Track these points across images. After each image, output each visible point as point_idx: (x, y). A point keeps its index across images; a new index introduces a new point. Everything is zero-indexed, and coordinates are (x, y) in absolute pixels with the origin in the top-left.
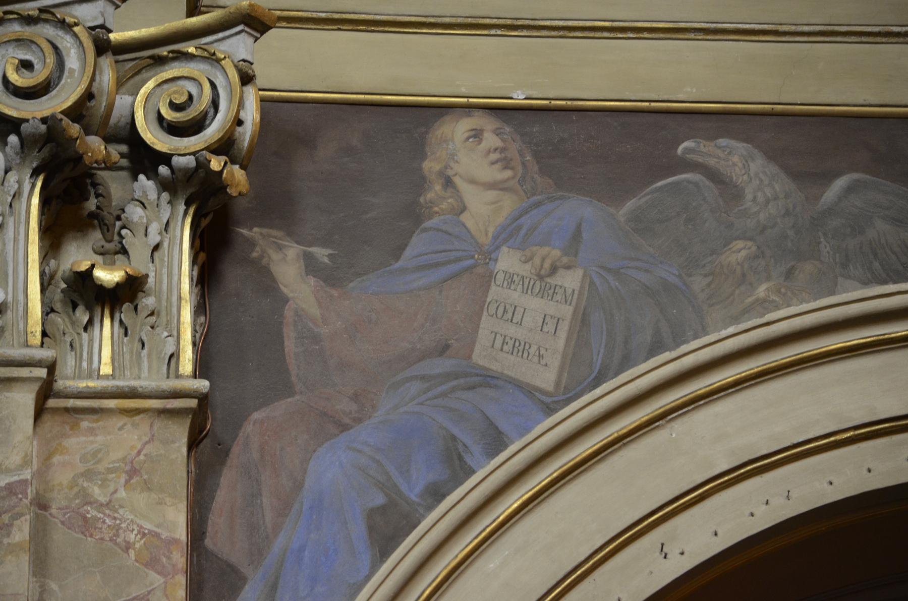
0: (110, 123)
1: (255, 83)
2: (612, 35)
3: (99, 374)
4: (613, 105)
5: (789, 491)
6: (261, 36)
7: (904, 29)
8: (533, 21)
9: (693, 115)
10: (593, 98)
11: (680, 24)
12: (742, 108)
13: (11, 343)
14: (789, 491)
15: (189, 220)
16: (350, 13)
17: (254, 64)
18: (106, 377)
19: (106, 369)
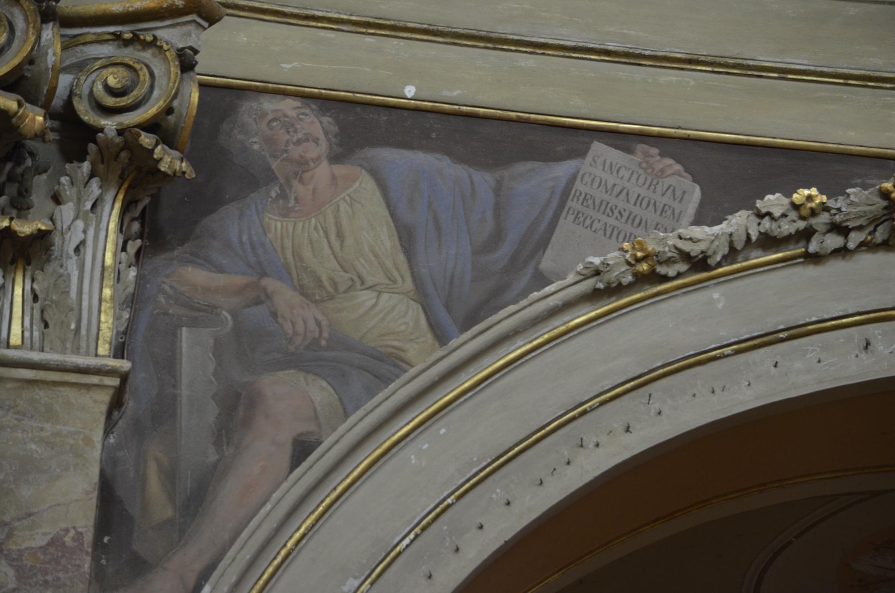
0: (53, 103)
1: (194, 70)
2: (393, 33)
3: (8, 343)
4: (787, 143)
5: (555, 469)
6: (209, 26)
7: (892, 75)
8: (775, 63)
9: (490, 120)
10: (386, 95)
11: (748, 61)
12: (236, 83)
13: (73, 326)
14: (555, 469)
15: (118, 205)
16: (365, 17)
17: (199, 54)
18: (16, 347)
19: (15, 339)
